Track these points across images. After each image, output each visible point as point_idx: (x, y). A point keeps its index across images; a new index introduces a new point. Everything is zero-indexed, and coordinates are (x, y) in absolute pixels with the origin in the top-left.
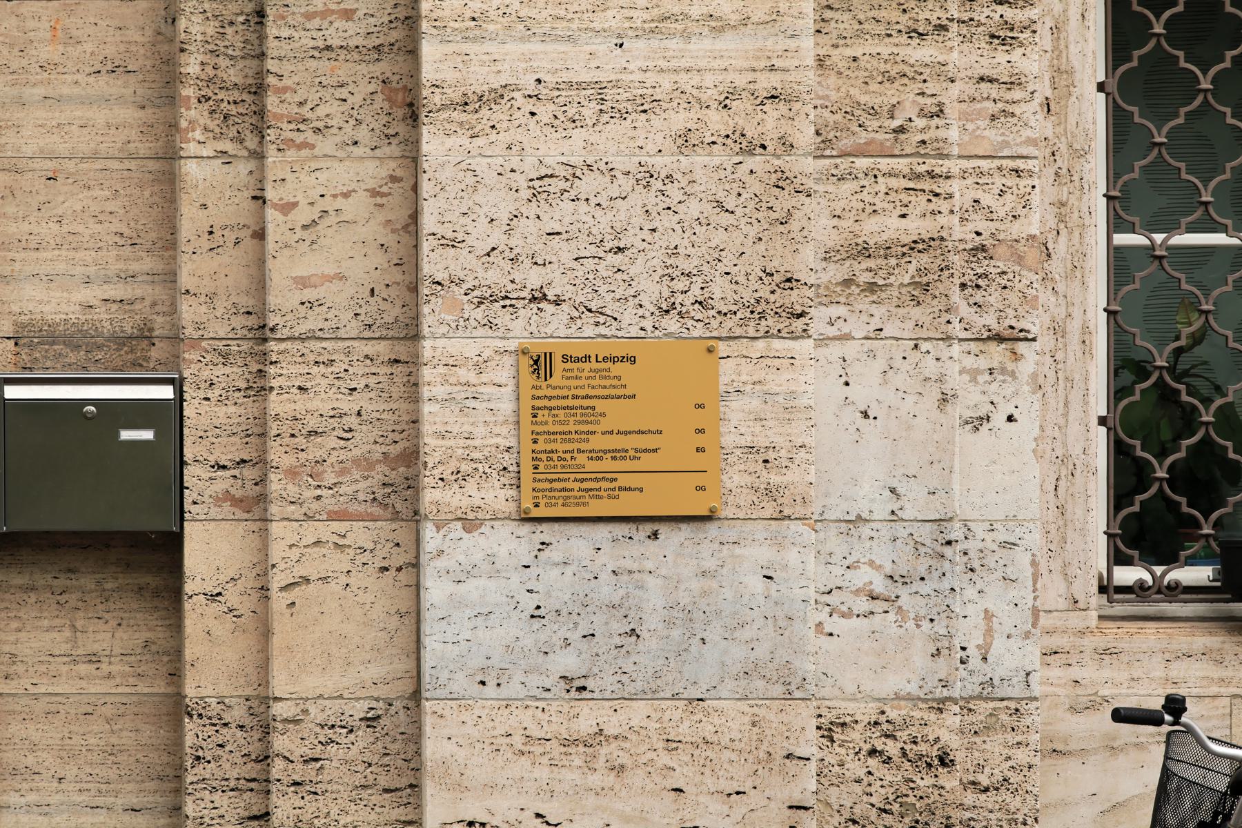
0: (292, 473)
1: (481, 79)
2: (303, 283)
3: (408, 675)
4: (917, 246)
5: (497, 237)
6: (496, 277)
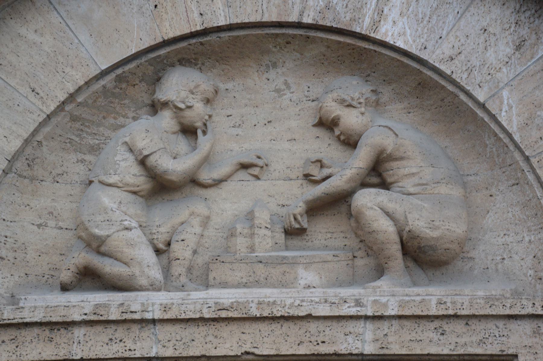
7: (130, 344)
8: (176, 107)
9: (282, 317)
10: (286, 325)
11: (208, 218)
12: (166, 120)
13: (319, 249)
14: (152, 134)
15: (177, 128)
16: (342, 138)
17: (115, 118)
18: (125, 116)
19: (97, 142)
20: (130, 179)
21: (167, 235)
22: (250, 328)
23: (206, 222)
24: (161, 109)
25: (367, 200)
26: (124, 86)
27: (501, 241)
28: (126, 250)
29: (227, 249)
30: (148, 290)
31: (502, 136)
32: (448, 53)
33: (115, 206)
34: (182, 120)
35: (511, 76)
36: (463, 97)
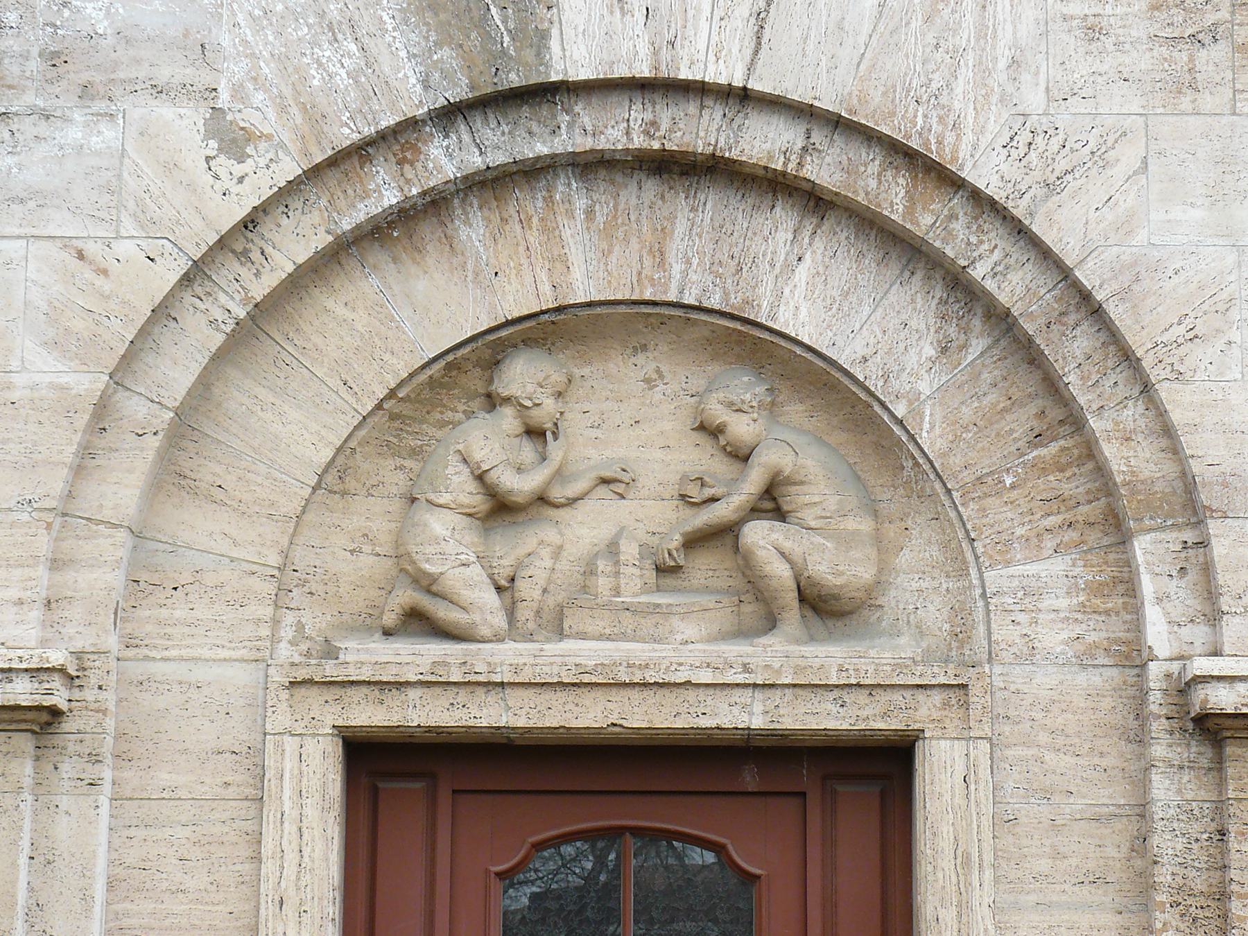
7: (475, 712)
8: (521, 405)
9: (656, 683)
10: (661, 692)
11: (561, 547)
12: (508, 420)
13: (697, 591)
14: (489, 441)
15: (521, 430)
16: (729, 449)
17: (442, 413)
18: (455, 410)
19: (420, 443)
20: (465, 499)
21: (510, 569)
22: (615, 695)
23: (558, 552)
24: (501, 405)
25: (760, 536)
26: (454, 373)
27: (915, 585)
28: (465, 592)
29: (584, 589)
30: (491, 641)
31: (921, 461)
32: (861, 352)
33: (448, 533)
34: (528, 421)
35: (935, 387)
36: (877, 408)
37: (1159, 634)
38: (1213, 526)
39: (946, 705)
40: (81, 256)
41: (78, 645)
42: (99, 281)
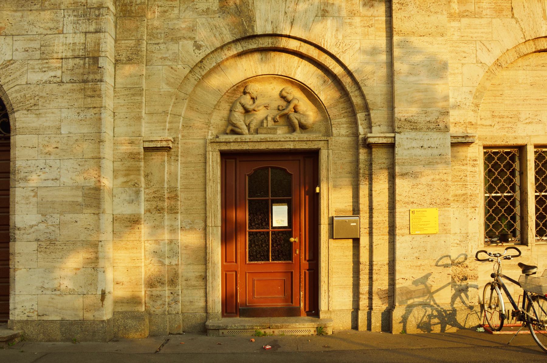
0: (376, 229)
1: (404, 171)
2: (378, 202)
3: (201, 161)
4: (463, 195)
5: (407, 194)
6: (406, 200)
22: (267, 143)
37: (361, 130)
38: (371, 112)
39: (325, 144)
40: (172, 68)
41: (174, 137)
42: (175, 72)
